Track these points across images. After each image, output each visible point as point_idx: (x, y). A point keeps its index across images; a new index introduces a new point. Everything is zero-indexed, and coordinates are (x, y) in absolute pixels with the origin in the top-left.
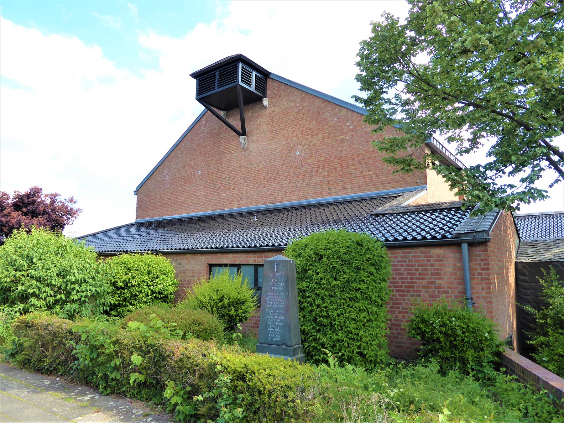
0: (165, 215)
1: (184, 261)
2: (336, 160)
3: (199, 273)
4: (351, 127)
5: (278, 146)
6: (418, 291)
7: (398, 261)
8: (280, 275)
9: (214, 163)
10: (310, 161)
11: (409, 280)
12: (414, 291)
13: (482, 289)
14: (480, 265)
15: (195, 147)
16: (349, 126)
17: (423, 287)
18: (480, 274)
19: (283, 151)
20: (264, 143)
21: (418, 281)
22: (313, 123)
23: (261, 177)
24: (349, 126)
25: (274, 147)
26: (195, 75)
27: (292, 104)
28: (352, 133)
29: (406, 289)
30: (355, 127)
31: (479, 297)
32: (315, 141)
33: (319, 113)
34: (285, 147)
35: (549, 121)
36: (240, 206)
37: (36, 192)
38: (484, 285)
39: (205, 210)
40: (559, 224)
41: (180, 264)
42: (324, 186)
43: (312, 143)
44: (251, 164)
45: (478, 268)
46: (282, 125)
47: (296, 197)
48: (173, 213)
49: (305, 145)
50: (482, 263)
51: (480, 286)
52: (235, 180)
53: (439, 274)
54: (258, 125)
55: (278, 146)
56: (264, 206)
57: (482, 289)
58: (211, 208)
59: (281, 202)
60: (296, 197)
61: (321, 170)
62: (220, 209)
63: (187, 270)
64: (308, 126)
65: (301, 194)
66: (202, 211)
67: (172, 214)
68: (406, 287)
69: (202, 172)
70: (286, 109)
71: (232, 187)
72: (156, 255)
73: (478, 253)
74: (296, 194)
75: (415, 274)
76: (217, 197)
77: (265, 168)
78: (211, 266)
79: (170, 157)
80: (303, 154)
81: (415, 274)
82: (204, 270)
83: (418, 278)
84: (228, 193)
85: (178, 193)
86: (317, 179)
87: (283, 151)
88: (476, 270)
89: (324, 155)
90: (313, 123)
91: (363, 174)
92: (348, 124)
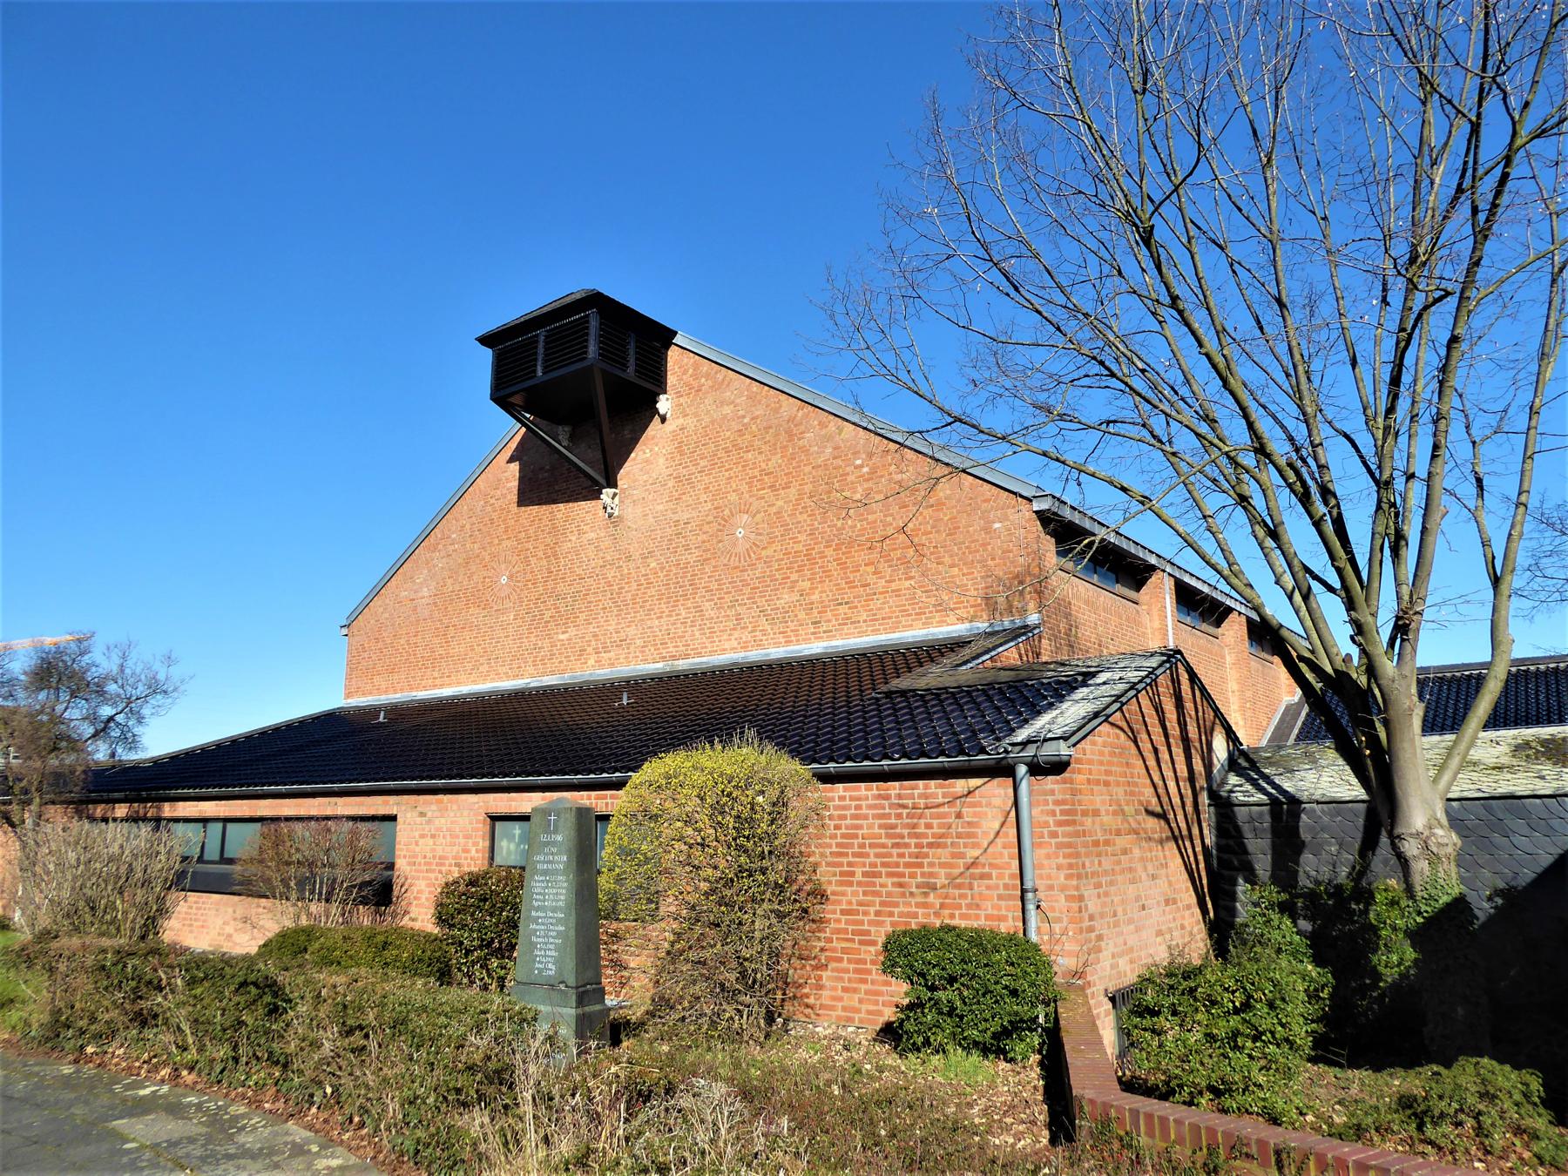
0: (417, 689)
1: (434, 807)
2: (829, 552)
3: (466, 837)
4: (866, 470)
5: (695, 514)
6: (931, 875)
7: (891, 806)
8: (559, 838)
9: (541, 554)
10: (769, 552)
11: (913, 850)
12: (923, 875)
13: (1059, 867)
14: (1053, 813)
15: (495, 516)
16: (861, 466)
17: (942, 865)
18: (1054, 835)
19: (706, 528)
20: (661, 507)
21: (931, 851)
22: (777, 459)
23: (653, 591)
24: (861, 466)
25: (686, 516)
26: (485, 340)
27: (727, 410)
28: (870, 484)
29: (907, 871)
30: (873, 471)
31: (1051, 888)
32: (780, 503)
33: (790, 435)
34: (710, 518)
36: (602, 667)
37: (83, 644)
38: (1061, 860)
39: (516, 676)
40: (1152, 763)
41: (422, 814)
42: (802, 615)
43: (774, 509)
44: (629, 558)
45: (1051, 820)
46: (703, 463)
47: (735, 644)
48: (438, 682)
49: (758, 512)
50: (1058, 809)
51: (1054, 862)
52: (591, 598)
53: (973, 835)
54: (647, 461)
55: (695, 514)
56: (660, 665)
57: (1059, 867)
58: (531, 670)
59: (699, 655)
60: (735, 644)
61: (794, 577)
62: (552, 673)
63: (439, 829)
64: (763, 466)
65: (746, 636)
66: (508, 678)
68: (907, 865)
69: (510, 577)
70: (713, 422)
71: (583, 616)
73: (1050, 786)
74: (736, 634)
75: (925, 836)
77: (662, 568)
78: (495, 818)
79: (432, 538)
80: (753, 536)
81: (925, 836)
82: (477, 830)
83: (930, 845)
84: (572, 632)
86: (786, 598)
87: (706, 528)
88: (1046, 824)
89: (802, 537)
90: (777, 459)
91: (894, 586)
92: (859, 462)
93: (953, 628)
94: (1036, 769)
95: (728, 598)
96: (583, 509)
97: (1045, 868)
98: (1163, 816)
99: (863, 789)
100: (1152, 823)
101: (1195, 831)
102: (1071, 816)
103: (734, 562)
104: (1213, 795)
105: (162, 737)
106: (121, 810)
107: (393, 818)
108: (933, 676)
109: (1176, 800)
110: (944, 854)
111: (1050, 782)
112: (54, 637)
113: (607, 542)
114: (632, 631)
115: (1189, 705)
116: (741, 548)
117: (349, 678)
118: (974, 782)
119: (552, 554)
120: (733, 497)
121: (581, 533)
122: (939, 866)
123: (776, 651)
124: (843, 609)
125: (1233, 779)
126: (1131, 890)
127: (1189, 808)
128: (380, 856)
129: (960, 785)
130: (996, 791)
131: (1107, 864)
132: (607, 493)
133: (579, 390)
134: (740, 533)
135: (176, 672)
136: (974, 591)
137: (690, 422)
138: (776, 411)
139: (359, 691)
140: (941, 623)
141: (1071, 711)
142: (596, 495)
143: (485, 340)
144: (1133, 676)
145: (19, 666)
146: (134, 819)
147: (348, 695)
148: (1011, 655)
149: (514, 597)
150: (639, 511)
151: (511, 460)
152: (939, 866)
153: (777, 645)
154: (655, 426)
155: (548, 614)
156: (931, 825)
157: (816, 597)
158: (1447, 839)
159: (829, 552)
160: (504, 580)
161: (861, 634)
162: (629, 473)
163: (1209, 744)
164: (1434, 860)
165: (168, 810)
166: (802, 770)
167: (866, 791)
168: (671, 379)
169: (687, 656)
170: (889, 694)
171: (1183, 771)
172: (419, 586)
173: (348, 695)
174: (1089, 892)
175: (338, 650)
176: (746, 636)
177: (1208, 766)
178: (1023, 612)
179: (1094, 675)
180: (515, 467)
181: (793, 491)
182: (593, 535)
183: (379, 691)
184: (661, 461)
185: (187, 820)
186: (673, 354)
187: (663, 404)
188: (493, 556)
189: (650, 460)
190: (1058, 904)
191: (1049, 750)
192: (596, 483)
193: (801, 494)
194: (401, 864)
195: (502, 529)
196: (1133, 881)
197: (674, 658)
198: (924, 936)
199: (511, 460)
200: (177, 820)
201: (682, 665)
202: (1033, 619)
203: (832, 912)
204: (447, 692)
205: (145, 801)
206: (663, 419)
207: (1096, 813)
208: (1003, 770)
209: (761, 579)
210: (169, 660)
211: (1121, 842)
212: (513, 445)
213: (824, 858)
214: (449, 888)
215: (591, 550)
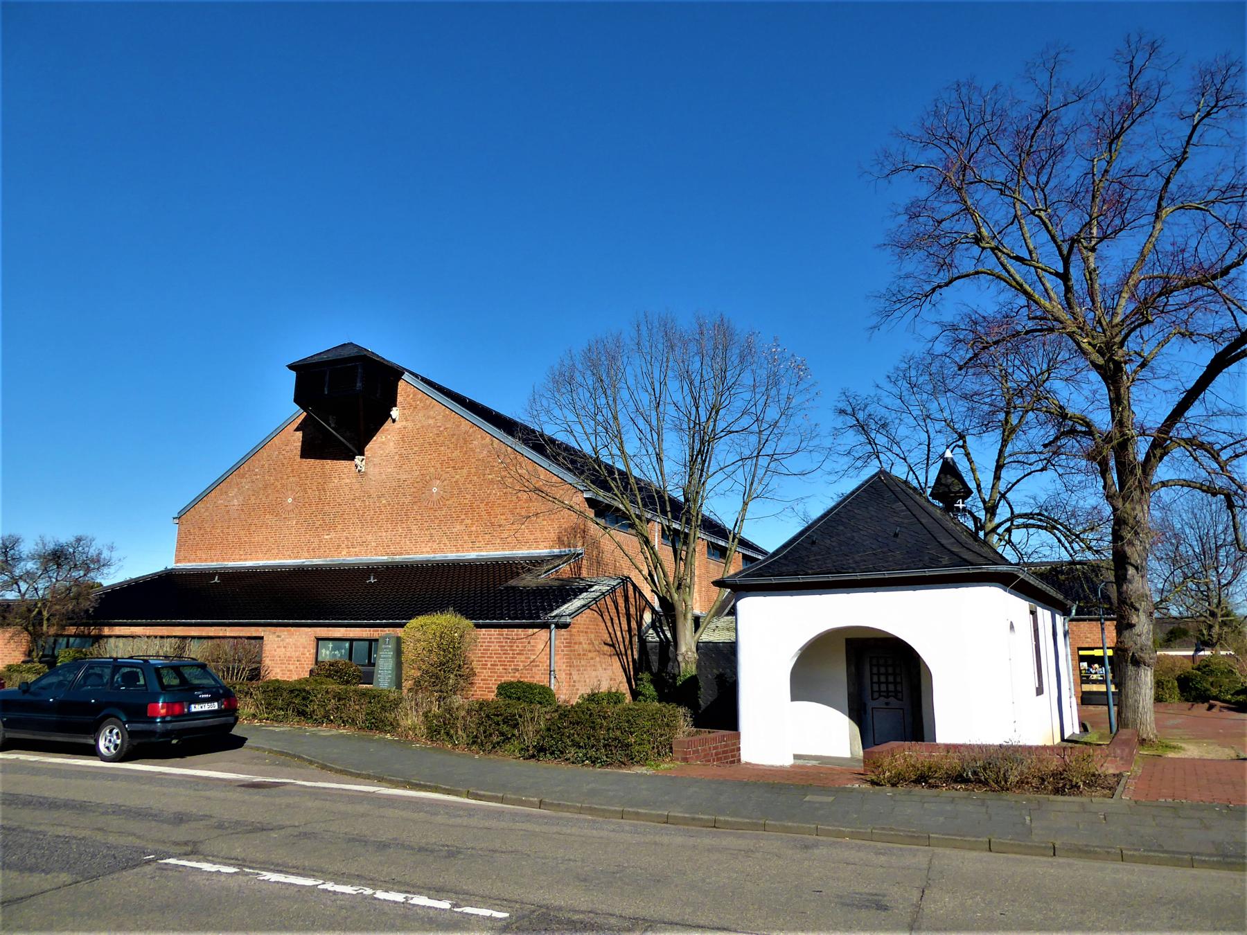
2: (482, 506)
15: (285, 462)
22: (457, 453)
26: (291, 367)
27: (431, 422)
33: (466, 441)
35: (896, 391)
39: (296, 558)
40: (609, 624)
42: (466, 538)
58: (306, 554)
69: (294, 499)
72: (894, 785)
76: (316, 540)
78: (318, 639)
84: (333, 535)
85: (253, 528)
86: (458, 528)
93: (543, 551)
94: (558, 626)
95: (426, 524)
96: (343, 464)
97: (559, 663)
98: (613, 646)
100: (606, 648)
101: (629, 652)
102: (569, 644)
103: (431, 505)
104: (640, 637)
108: (528, 581)
109: (620, 639)
110: (523, 658)
111: (563, 631)
112: (63, 536)
113: (357, 486)
114: (369, 538)
115: (632, 600)
116: (435, 498)
117: (178, 550)
119: (322, 489)
120: (432, 470)
122: (520, 661)
123: (452, 556)
124: (487, 536)
125: (651, 631)
126: (594, 673)
127: (627, 642)
129: (530, 631)
130: (543, 634)
131: (583, 662)
132: (358, 459)
133: (344, 402)
134: (435, 490)
136: (553, 536)
137: (410, 425)
138: (458, 426)
139: (185, 559)
140: (537, 548)
141: (577, 603)
142: (353, 459)
143: (291, 367)
144: (605, 589)
147: (177, 562)
148: (565, 569)
149: (296, 511)
150: (377, 470)
151: (297, 430)
152: (520, 661)
153: (452, 552)
156: (518, 647)
157: (474, 529)
158: (693, 656)
159: (482, 506)
160: (290, 500)
161: (496, 550)
163: (641, 617)
164: (687, 663)
165: (106, 631)
166: (471, 623)
167: (494, 632)
168: (399, 399)
169: (401, 554)
170: (506, 588)
171: (625, 627)
172: (233, 498)
173: (177, 562)
174: (574, 673)
175: (172, 533)
176: (435, 546)
177: (640, 624)
178: (575, 547)
179: (591, 586)
180: (300, 434)
181: (465, 471)
186: (401, 384)
187: (395, 413)
188: (283, 486)
189: (384, 443)
190: (562, 676)
191: (563, 620)
192: (351, 451)
193: (469, 473)
194: (267, 662)
195: (289, 470)
197: (394, 554)
198: (510, 684)
199: (297, 430)
201: (398, 558)
202: (579, 550)
203: (477, 680)
208: (546, 626)
209: (445, 516)
210: (111, 548)
211: (590, 655)
212: (299, 421)
213: (475, 658)
215: (347, 490)
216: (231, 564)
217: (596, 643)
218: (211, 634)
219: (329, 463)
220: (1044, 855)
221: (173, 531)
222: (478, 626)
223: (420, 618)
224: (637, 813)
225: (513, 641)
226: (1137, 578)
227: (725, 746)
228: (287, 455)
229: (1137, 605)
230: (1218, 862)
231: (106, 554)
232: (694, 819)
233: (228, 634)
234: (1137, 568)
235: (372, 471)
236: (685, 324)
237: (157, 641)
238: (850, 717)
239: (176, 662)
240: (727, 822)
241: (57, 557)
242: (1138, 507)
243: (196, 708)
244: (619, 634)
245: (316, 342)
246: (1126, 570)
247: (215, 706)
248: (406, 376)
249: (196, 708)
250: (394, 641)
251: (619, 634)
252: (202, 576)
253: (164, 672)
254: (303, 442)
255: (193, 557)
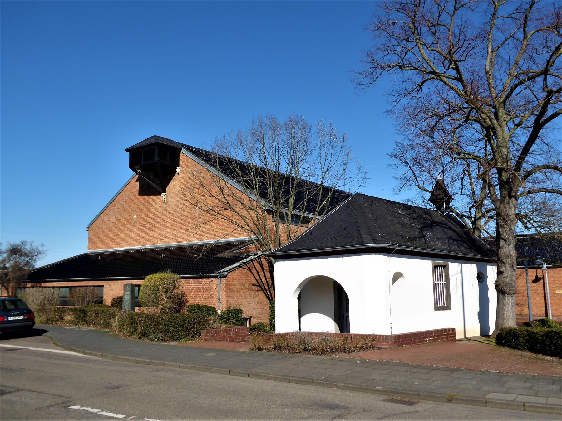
15: (132, 197)
23: (175, 223)
26: (127, 150)
39: (138, 245)
40: (256, 275)
42: (212, 232)
54: (174, 186)
62: (148, 245)
66: (136, 246)
67: (115, 247)
69: (137, 216)
71: (157, 229)
79: (114, 203)
84: (154, 233)
85: (120, 231)
98: (260, 286)
99: (195, 280)
100: (254, 287)
105: (40, 263)
106: (29, 285)
107: (103, 286)
110: (207, 293)
112: (16, 241)
113: (164, 208)
114: (169, 234)
118: (212, 279)
121: (156, 205)
128: (100, 295)
129: (210, 280)
133: (154, 164)
135: (44, 249)
142: (160, 194)
143: (127, 150)
145: (5, 247)
146: (33, 287)
147: (89, 249)
153: (206, 239)
154: (176, 176)
155: (147, 227)
156: (206, 287)
157: (215, 227)
160: (135, 217)
162: (169, 188)
168: (181, 162)
169: (183, 241)
172: (110, 217)
173: (89, 249)
182: (159, 206)
183: (98, 248)
184: (178, 186)
185: (49, 287)
186: (181, 155)
187: (178, 170)
189: (175, 185)
194: (105, 297)
196: (246, 298)
197: (180, 242)
200: (45, 287)
201: (182, 244)
204: (119, 249)
205: (36, 282)
206: (178, 174)
207: (235, 285)
208: (216, 277)
210: (42, 245)
214: (114, 300)
215: (159, 210)
216: (112, 250)
217: (246, 285)
218: (83, 285)
219: (151, 197)
220: (245, 377)
221: (86, 233)
222: (183, 278)
223: (152, 276)
224: (128, 359)
225: (203, 284)
226: (505, 245)
227: (236, 334)
228: (133, 194)
229: (504, 261)
230: (298, 380)
231: (40, 249)
232: (144, 361)
233: (90, 285)
234: (505, 241)
235: (170, 200)
236: (282, 120)
237: (51, 289)
238: (335, 321)
239: (13, 298)
240: (154, 363)
241: (15, 251)
242: (508, 206)
243: (10, 318)
244: (264, 280)
245: (138, 137)
246: (499, 241)
247: (22, 317)
248: (183, 151)
249: (10, 318)
250: (130, 286)
251: (264, 280)
252: (95, 255)
253: (7, 302)
254: (139, 187)
255: (95, 247)
